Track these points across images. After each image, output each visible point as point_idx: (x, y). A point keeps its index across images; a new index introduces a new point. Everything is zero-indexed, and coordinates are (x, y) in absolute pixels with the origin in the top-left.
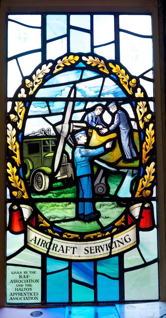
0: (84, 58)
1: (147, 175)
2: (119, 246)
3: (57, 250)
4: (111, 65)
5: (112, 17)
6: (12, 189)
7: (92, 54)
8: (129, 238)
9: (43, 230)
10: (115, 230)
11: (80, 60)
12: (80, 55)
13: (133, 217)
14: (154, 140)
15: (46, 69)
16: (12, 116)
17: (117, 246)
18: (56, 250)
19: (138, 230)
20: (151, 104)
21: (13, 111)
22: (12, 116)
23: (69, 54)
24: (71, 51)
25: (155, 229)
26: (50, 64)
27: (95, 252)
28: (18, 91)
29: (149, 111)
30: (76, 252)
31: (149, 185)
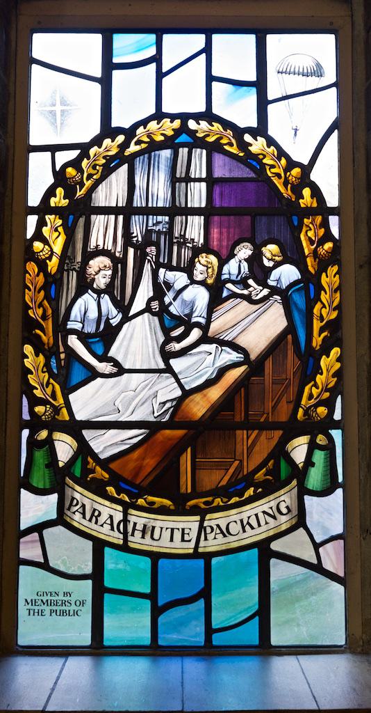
0: (192, 124)
1: (322, 374)
2: (267, 523)
3: (99, 523)
4: (247, 138)
5: (251, 38)
6: (35, 401)
7: (208, 116)
8: (287, 507)
9: (98, 488)
10: (251, 491)
11: (184, 129)
12: (184, 117)
13: (291, 462)
14: (338, 299)
15: (111, 146)
16: (38, 246)
17: (263, 522)
18: (96, 523)
19: (303, 491)
20: (334, 222)
21: (39, 236)
22: (38, 246)
23: (159, 115)
24: (166, 109)
25: (339, 492)
26: (121, 139)
27: (241, 531)
28: (50, 192)
29: (328, 236)
30: (31, 187)
31: (327, 395)
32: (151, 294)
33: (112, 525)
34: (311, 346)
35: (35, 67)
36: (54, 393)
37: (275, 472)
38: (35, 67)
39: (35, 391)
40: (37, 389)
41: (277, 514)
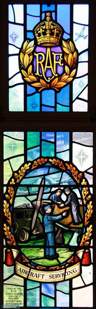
0: (50, 160)
9: (25, 264)
11: (48, 161)
12: (48, 158)
13: (78, 258)
16: (7, 196)
17: (69, 274)
19: (81, 265)
20: (91, 189)
22: (7, 196)
23: (41, 157)
25: (92, 266)
26: (30, 164)
28: (10, 180)
29: (90, 194)
32: (87, 72)
33: (36, 276)
34: (85, 225)
35: (4, 136)
36: (12, 237)
37: (74, 260)
38: (4, 136)
39: (4, 228)
40: (5, 228)
41: (73, 272)
